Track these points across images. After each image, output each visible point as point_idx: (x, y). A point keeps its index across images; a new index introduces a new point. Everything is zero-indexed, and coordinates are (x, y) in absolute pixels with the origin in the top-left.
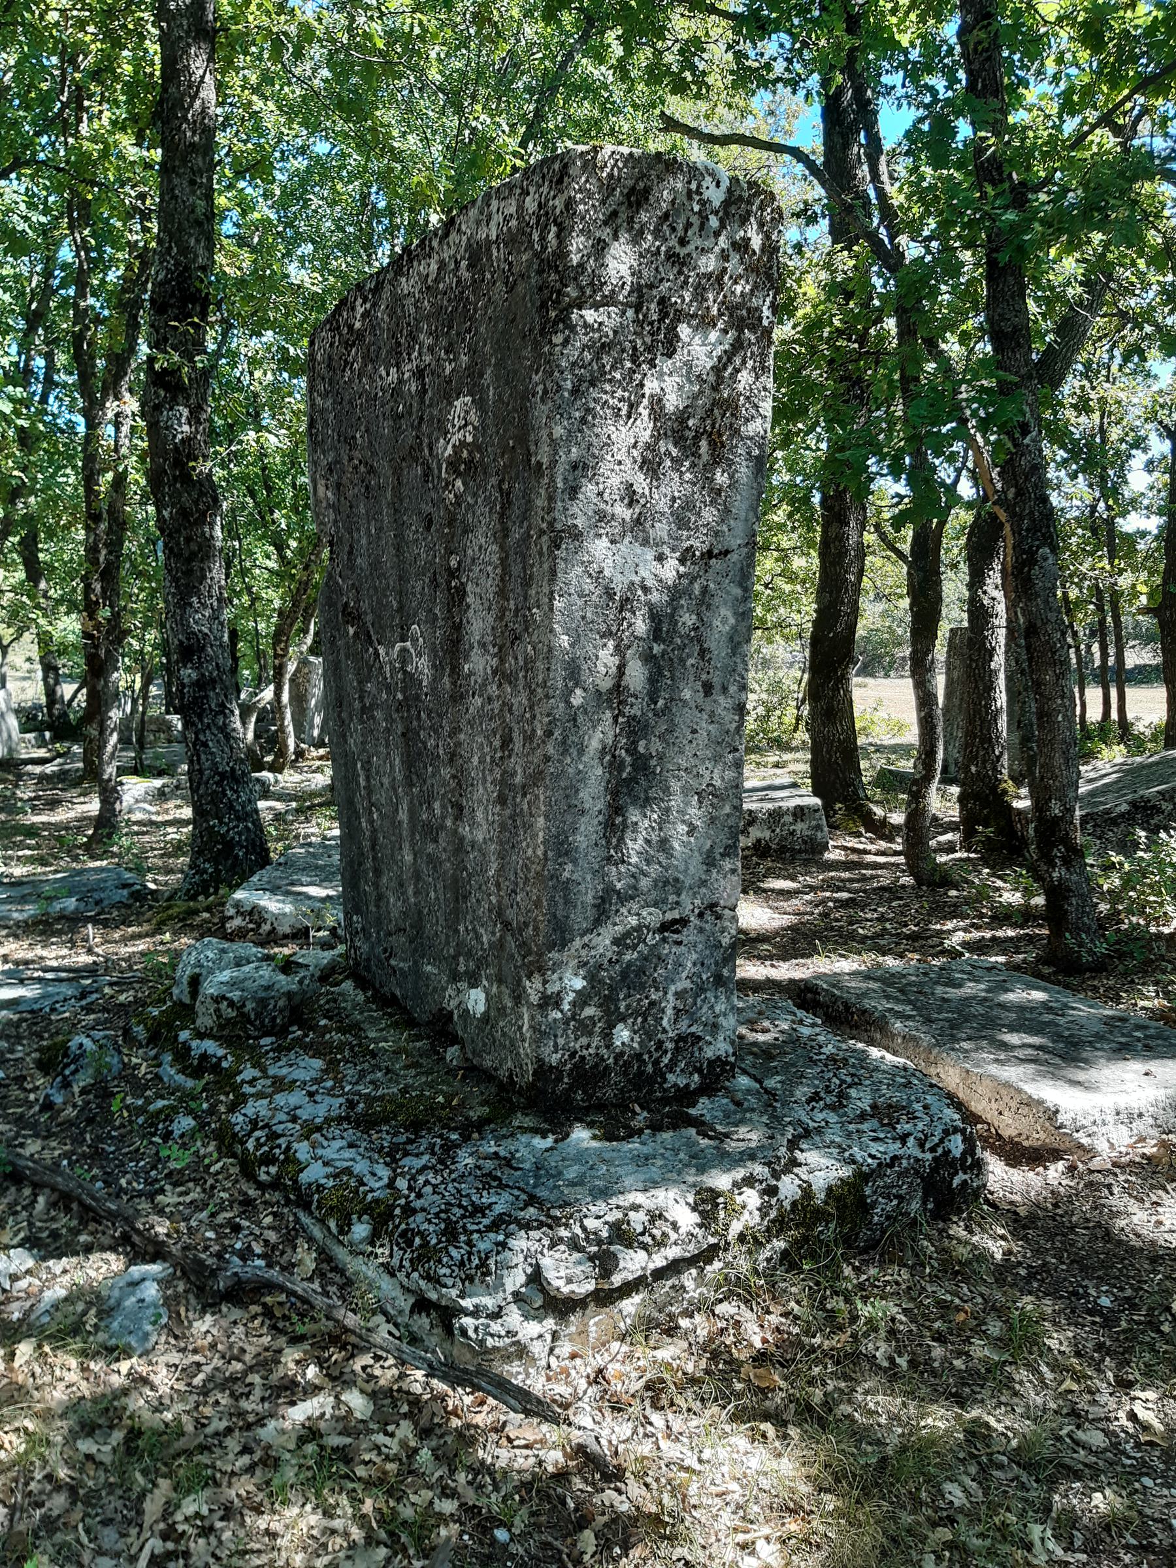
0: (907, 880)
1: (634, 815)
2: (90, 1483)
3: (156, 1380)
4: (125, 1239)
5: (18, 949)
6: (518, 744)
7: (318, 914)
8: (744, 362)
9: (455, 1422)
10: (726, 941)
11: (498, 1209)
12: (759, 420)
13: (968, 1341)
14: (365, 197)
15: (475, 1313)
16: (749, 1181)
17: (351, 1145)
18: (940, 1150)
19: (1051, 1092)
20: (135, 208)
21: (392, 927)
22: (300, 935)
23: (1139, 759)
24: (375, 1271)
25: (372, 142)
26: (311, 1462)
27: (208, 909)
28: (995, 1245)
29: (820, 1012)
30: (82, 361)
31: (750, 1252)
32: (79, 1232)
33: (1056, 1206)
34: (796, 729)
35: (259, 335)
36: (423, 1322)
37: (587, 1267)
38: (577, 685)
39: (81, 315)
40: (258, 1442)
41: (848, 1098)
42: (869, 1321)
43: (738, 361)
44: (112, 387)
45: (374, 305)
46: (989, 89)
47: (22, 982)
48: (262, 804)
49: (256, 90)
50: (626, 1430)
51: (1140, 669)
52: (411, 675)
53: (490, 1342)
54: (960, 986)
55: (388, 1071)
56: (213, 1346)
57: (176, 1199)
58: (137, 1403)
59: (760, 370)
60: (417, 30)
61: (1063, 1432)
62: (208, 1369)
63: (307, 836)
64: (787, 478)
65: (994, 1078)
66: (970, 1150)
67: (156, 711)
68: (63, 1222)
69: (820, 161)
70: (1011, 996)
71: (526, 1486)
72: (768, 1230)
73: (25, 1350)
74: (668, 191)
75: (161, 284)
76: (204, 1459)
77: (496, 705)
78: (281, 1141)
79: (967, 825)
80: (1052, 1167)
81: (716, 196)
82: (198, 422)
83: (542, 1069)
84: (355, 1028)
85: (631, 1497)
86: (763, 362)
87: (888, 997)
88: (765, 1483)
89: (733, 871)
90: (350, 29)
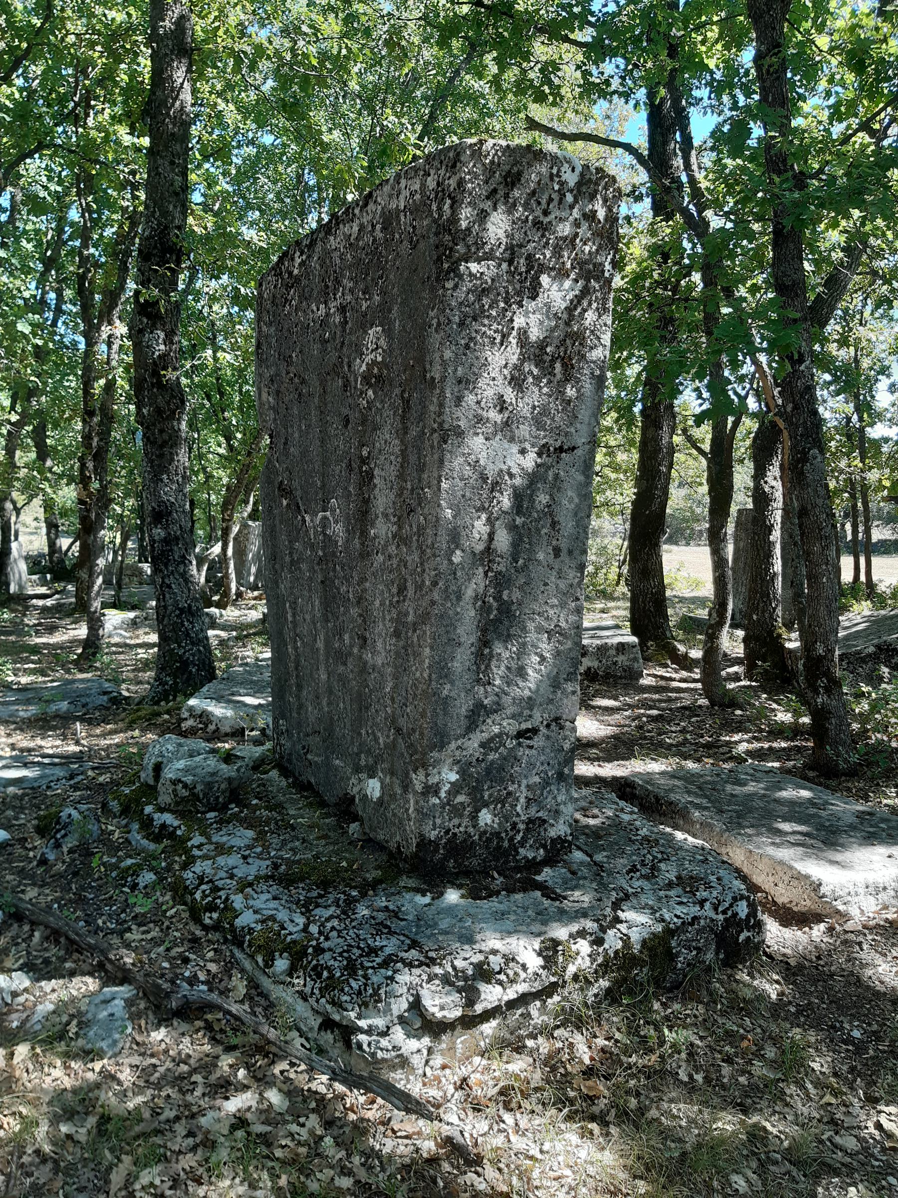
0: (703, 702)
1: (498, 648)
2: (69, 1158)
3: (122, 1077)
4: (101, 966)
5: (23, 740)
6: (410, 592)
7: (252, 719)
8: (590, 304)
9: (352, 1117)
10: (567, 746)
11: (388, 951)
12: (601, 349)
13: (750, 1062)
14: (300, 177)
15: (369, 1032)
16: (582, 934)
17: (275, 898)
18: (730, 913)
19: (815, 869)
20: (128, 182)
21: (309, 730)
22: (238, 734)
23: (883, 612)
24: (292, 996)
25: (307, 135)
26: (241, 1145)
27: (168, 712)
28: (771, 988)
29: (636, 802)
30: (83, 294)
31: (582, 989)
32: (65, 960)
33: (819, 958)
34: (618, 584)
35: (217, 278)
36: (328, 1037)
37: (456, 997)
38: (457, 547)
39: (84, 260)
40: (200, 1128)
41: (659, 870)
42: (673, 1045)
43: (585, 303)
44: (106, 316)
45: (309, 257)
46: (777, 100)
47: (26, 765)
48: (211, 633)
49: (219, 95)
50: (483, 1126)
51: (883, 542)
52: (330, 537)
53: (380, 1054)
54: (745, 785)
55: (304, 841)
56: (166, 1051)
57: (140, 937)
58: (109, 1097)
59: (602, 310)
60: (344, 52)
61: (824, 1137)
62: (162, 1069)
63: (243, 658)
64: (614, 393)
65: (771, 858)
66: (753, 913)
67: (129, 561)
68: (54, 952)
69: (646, 153)
70: (784, 794)
71: (406, 1168)
72: (596, 972)
73: (22, 1050)
74: (534, 174)
75: (147, 239)
76: (158, 1140)
77: (395, 561)
78: (221, 893)
79: (749, 661)
80: (816, 928)
81: (571, 179)
82: (172, 343)
83: (424, 843)
84: (279, 807)
86: (604, 304)
87: (689, 793)
88: (591, 1170)
89: (574, 693)
90: (293, 50)
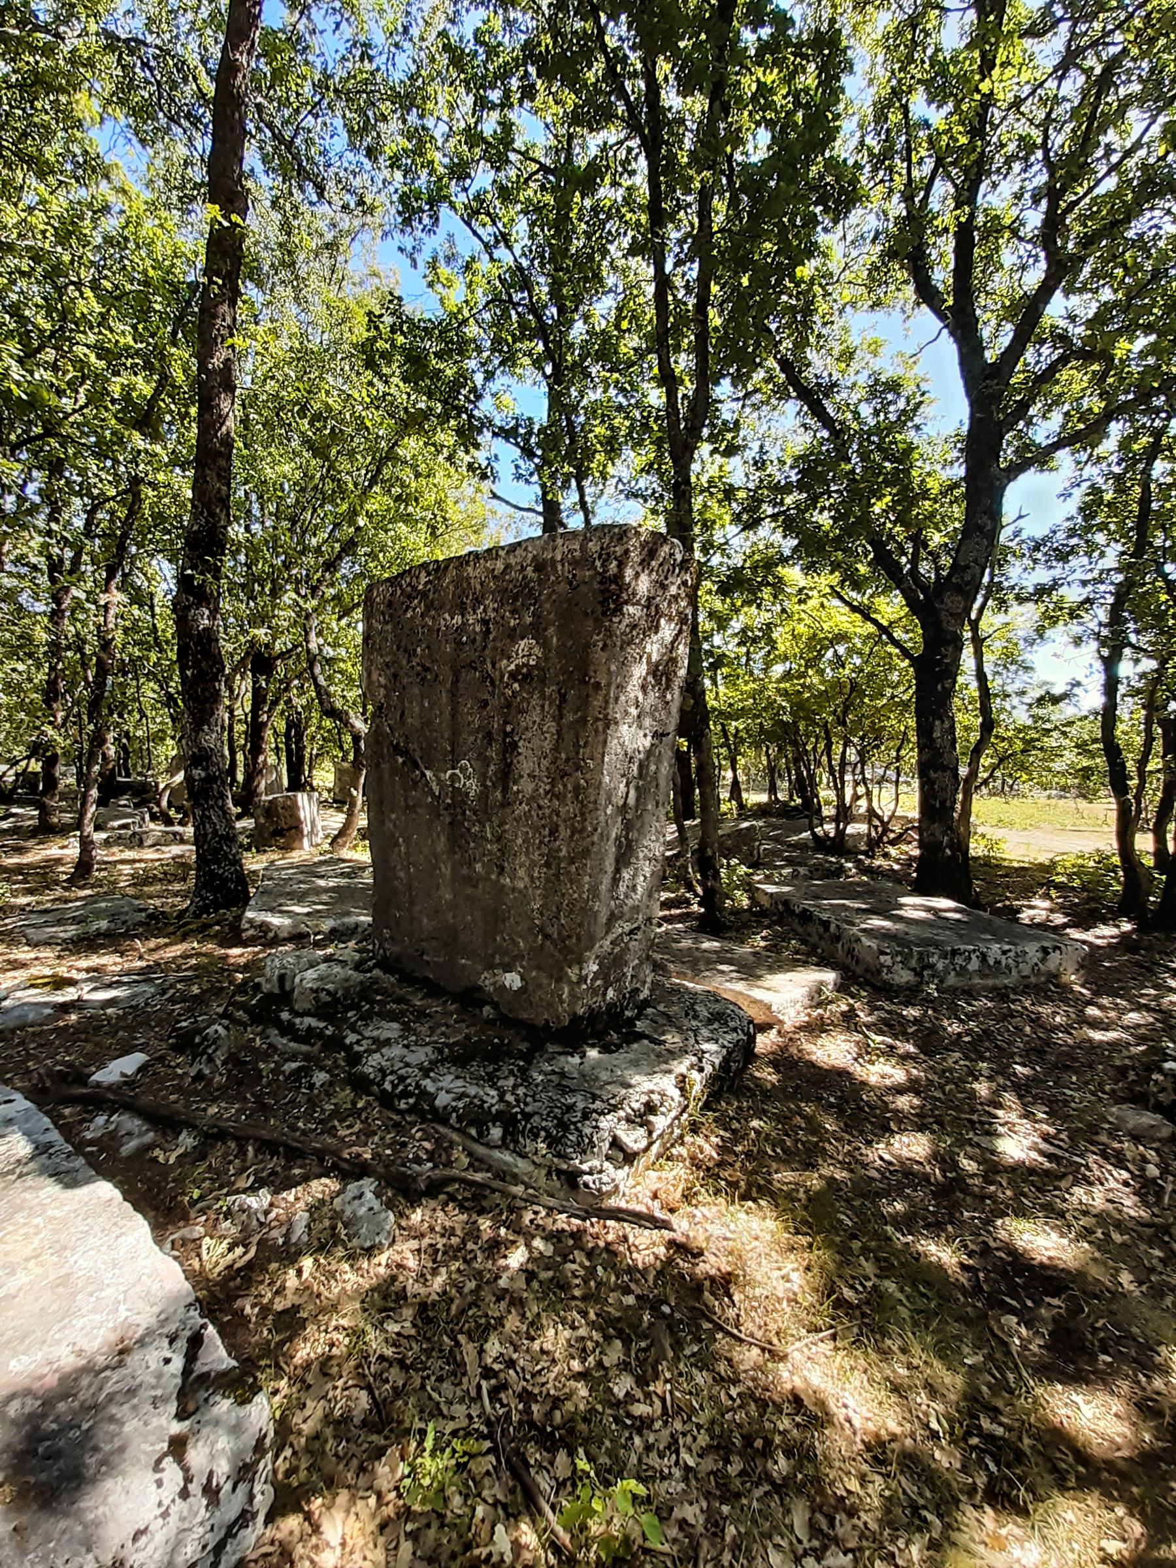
6: (564, 832)
68: (274, 1163)
73: (307, 1263)
83: (575, 1019)
85: (711, 1265)
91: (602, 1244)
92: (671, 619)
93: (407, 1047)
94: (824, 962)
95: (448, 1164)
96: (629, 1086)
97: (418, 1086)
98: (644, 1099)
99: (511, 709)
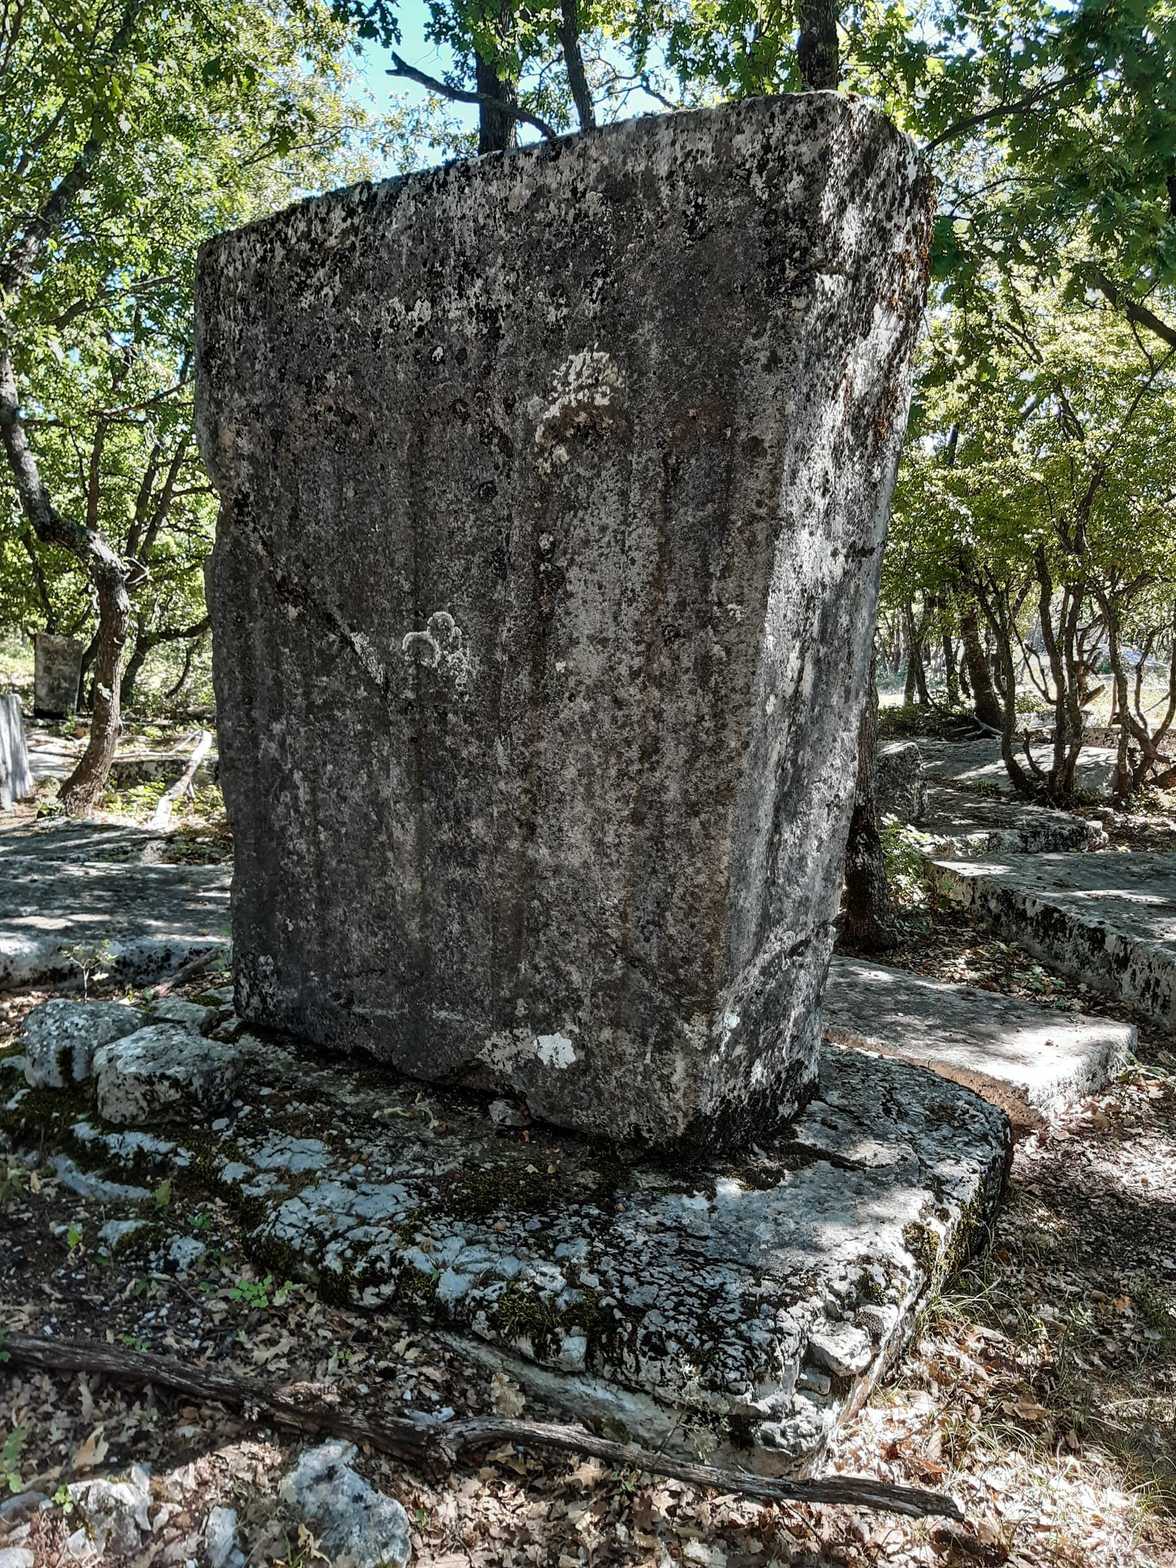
6: (674, 753)
17: (470, 1243)
68: (138, 1417)
83: (698, 1122)
91: (814, 1547)
92: (891, 307)
93: (352, 1185)
94: (1100, 1007)
95: (484, 1409)
96: (818, 1249)
97: (395, 1261)
98: (855, 1274)
99: (553, 501)
